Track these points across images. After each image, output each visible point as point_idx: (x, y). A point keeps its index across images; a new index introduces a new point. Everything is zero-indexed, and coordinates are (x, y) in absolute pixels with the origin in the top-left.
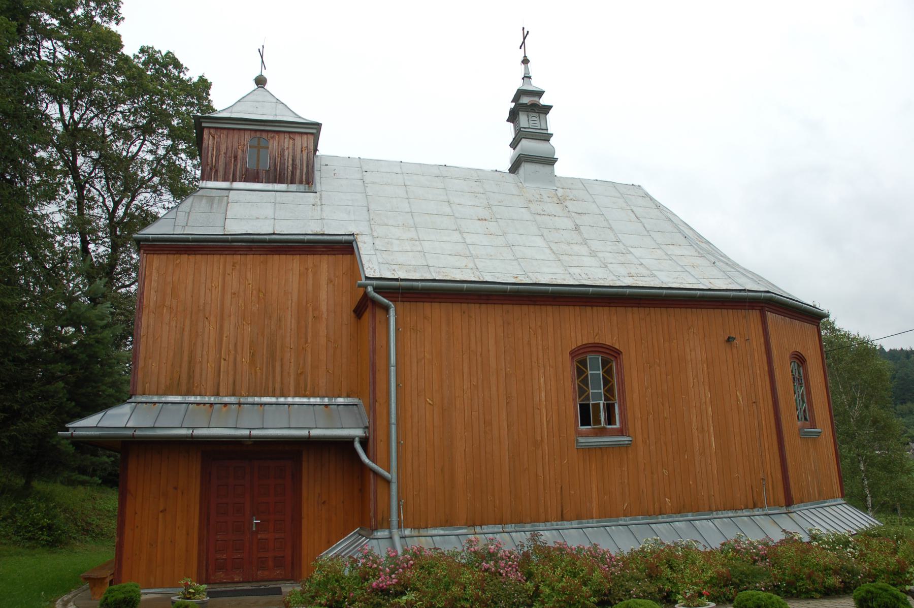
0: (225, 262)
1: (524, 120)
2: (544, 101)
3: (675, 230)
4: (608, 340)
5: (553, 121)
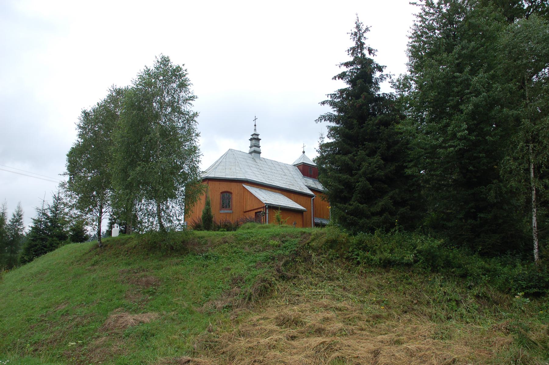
1: (254, 141)
5: (261, 143)
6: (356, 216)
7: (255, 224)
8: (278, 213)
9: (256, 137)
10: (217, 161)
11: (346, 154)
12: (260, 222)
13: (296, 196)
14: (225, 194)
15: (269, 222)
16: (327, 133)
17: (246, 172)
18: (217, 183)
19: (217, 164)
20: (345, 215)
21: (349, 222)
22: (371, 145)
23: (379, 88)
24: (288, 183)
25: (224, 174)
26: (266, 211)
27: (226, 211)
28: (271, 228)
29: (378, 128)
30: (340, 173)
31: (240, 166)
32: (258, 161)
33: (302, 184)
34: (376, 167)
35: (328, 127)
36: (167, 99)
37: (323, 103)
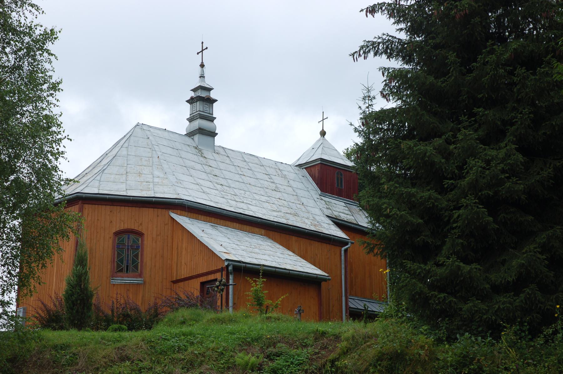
0: (129, 238)
1: (199, 106)
2: (213, 95)
3: (98, 178)
4: (135, 227)
5: (217, 110)
7: (201, 311)
8: (257, 285)
9: (204, 94)
10: (106, 154)
11: (426, 138)
12: (213, 306)
13: (304, 243)
14: (125, 236)
17: (179, 181)
18: (105, 210)
19: (105, 162)
22: (490, 114)
24: (284, 210)
25: (123, 186)
28: (242, 322)
30: (413, 185)
31: (165, 166)
32: (208, 154)
33: (317, 213)
35: (384, 70)
37: (372, 10)
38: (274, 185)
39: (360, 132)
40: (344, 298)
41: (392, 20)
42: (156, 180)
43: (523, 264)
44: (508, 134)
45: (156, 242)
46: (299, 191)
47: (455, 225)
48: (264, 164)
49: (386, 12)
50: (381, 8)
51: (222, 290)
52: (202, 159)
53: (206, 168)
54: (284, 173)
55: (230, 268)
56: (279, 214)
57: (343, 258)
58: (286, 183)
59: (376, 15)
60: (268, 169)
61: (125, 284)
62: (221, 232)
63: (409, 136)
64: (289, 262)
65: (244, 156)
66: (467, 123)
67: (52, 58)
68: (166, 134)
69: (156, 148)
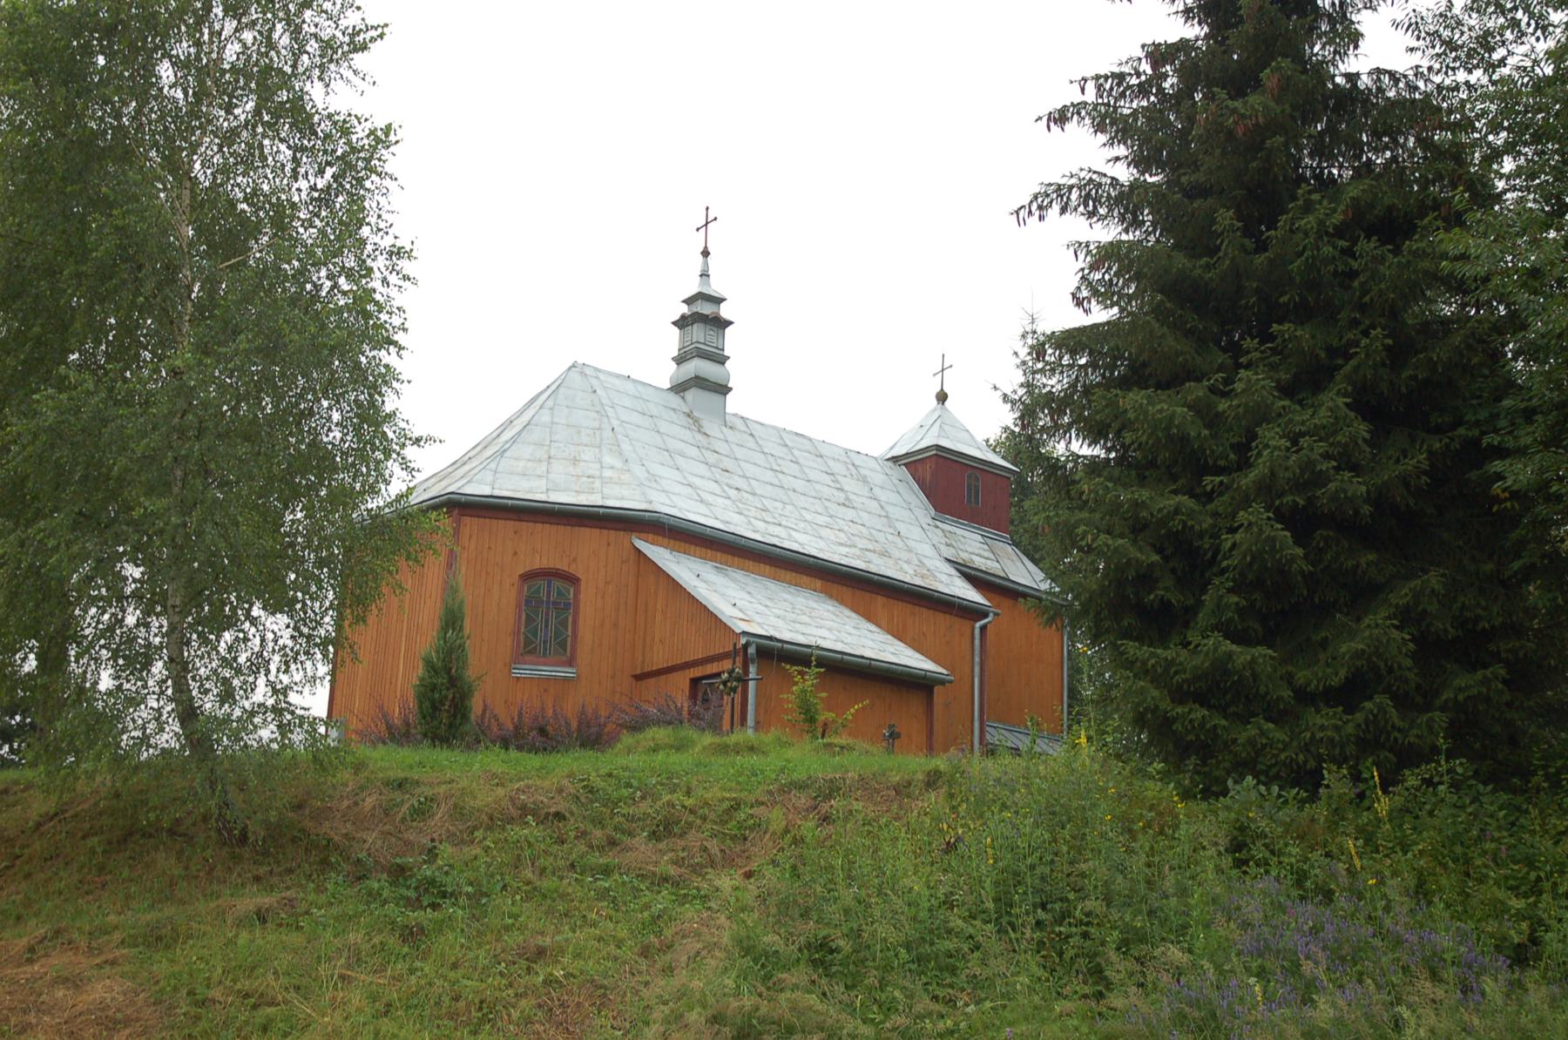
1: (698, 332)
2: (725, 311)
3: (493, 466)
5: (732, 341)
6: (1223, 710)
7: (689, 732)
8: (808, 681)
9: (706, 309)
11: (1170, 382)
12: (715, 727)
13: (900, 609)
14: (542, 584)
15: (758, 726)
16: (1075, 281)
17: (654, 478)
20: (1165, 705)
21: (1193, 738)
22: (1299, 335)
23: (1355, 38)
24: (862, 543)
25: (542, 484)
26: (746, 672)
27: (546, 671)
28: (772, 755)
29: (1349, 252)
30: (1142, 480)
31: (626, 447)
32: (712, 427)
33: (928, 551)
34: (1327, 456)
35: (1079, 247)
36: (232, 51)
37: (1060, 118)
38: (842, 495)
39: (1013, 403)
40: (977, 724)
41: (1102, 138)
42: (607, 473)
43: (1363, 651)
44: (1338, 378)
45: (603, 597)
46: (890, 509)
47: (1225, 564)
48: (824, 452)
49: (1088, 121)
50: (1079, 113)
51: (734, 690)
52: (699, 437)
53: (708, 454)
54: (863, 472)
55: (752, 650)
56: (852, 550)
57: (977, 642)
58: (866, 492)
59: (1067, 126)
60: (831, 463)
61: (541, 679)
62: (734, 580)
63: (1125, 383)
64: (870, 643)
65: (784, 435)
66: (1257, 355)
67: (387, 182)
68: (629, 386)
69: (610, 412)
